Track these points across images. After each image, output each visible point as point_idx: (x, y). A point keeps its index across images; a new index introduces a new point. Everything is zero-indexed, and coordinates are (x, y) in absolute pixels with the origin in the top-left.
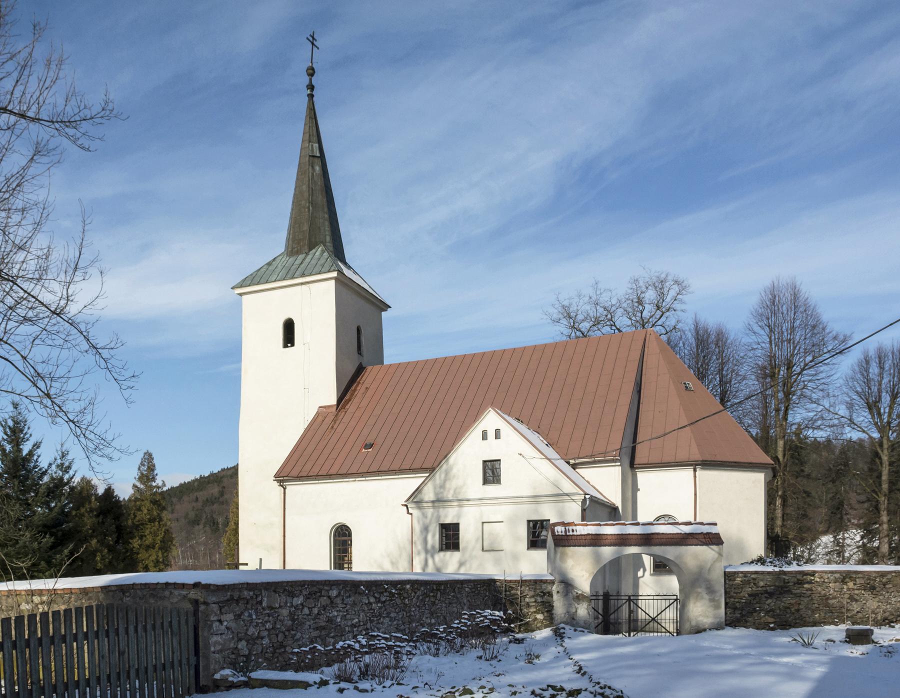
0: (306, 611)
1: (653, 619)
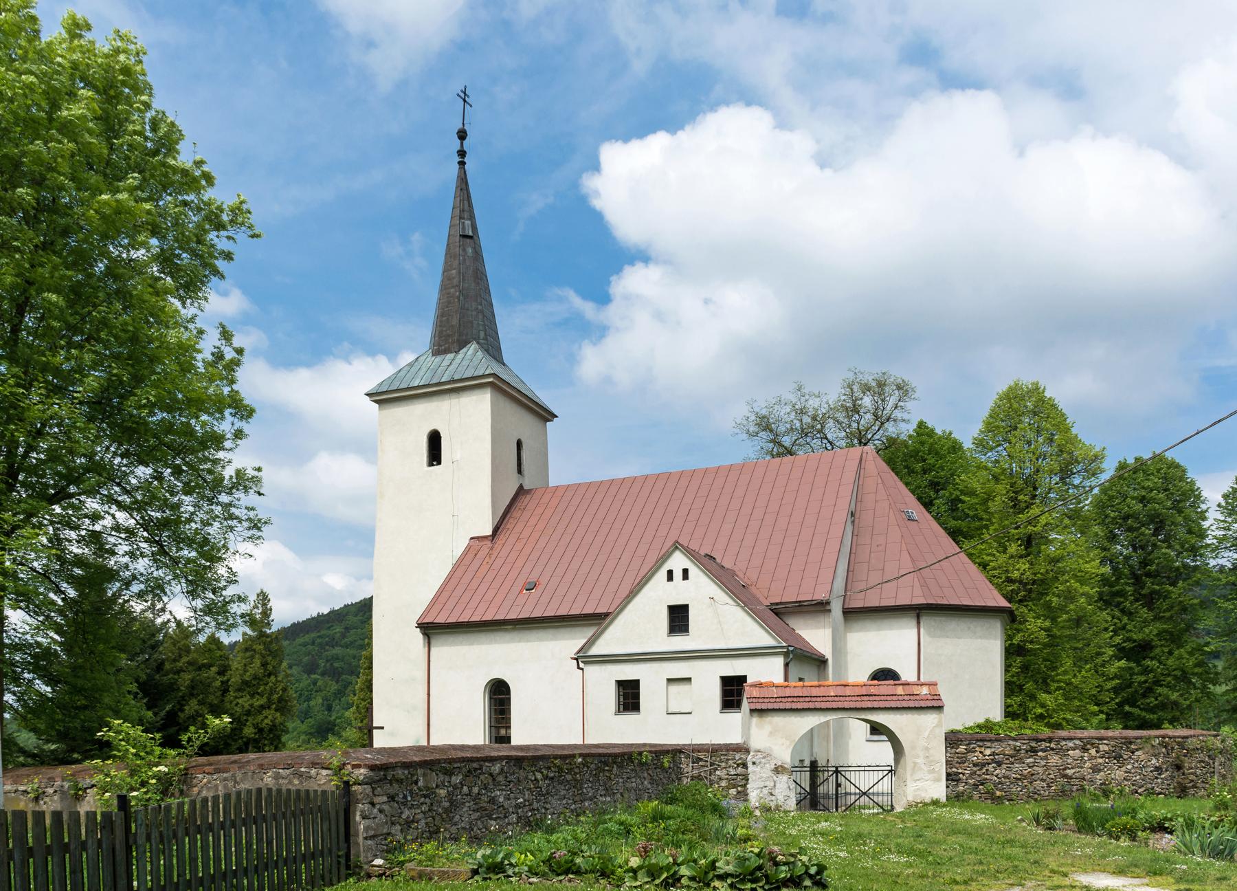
1: (864, 794)
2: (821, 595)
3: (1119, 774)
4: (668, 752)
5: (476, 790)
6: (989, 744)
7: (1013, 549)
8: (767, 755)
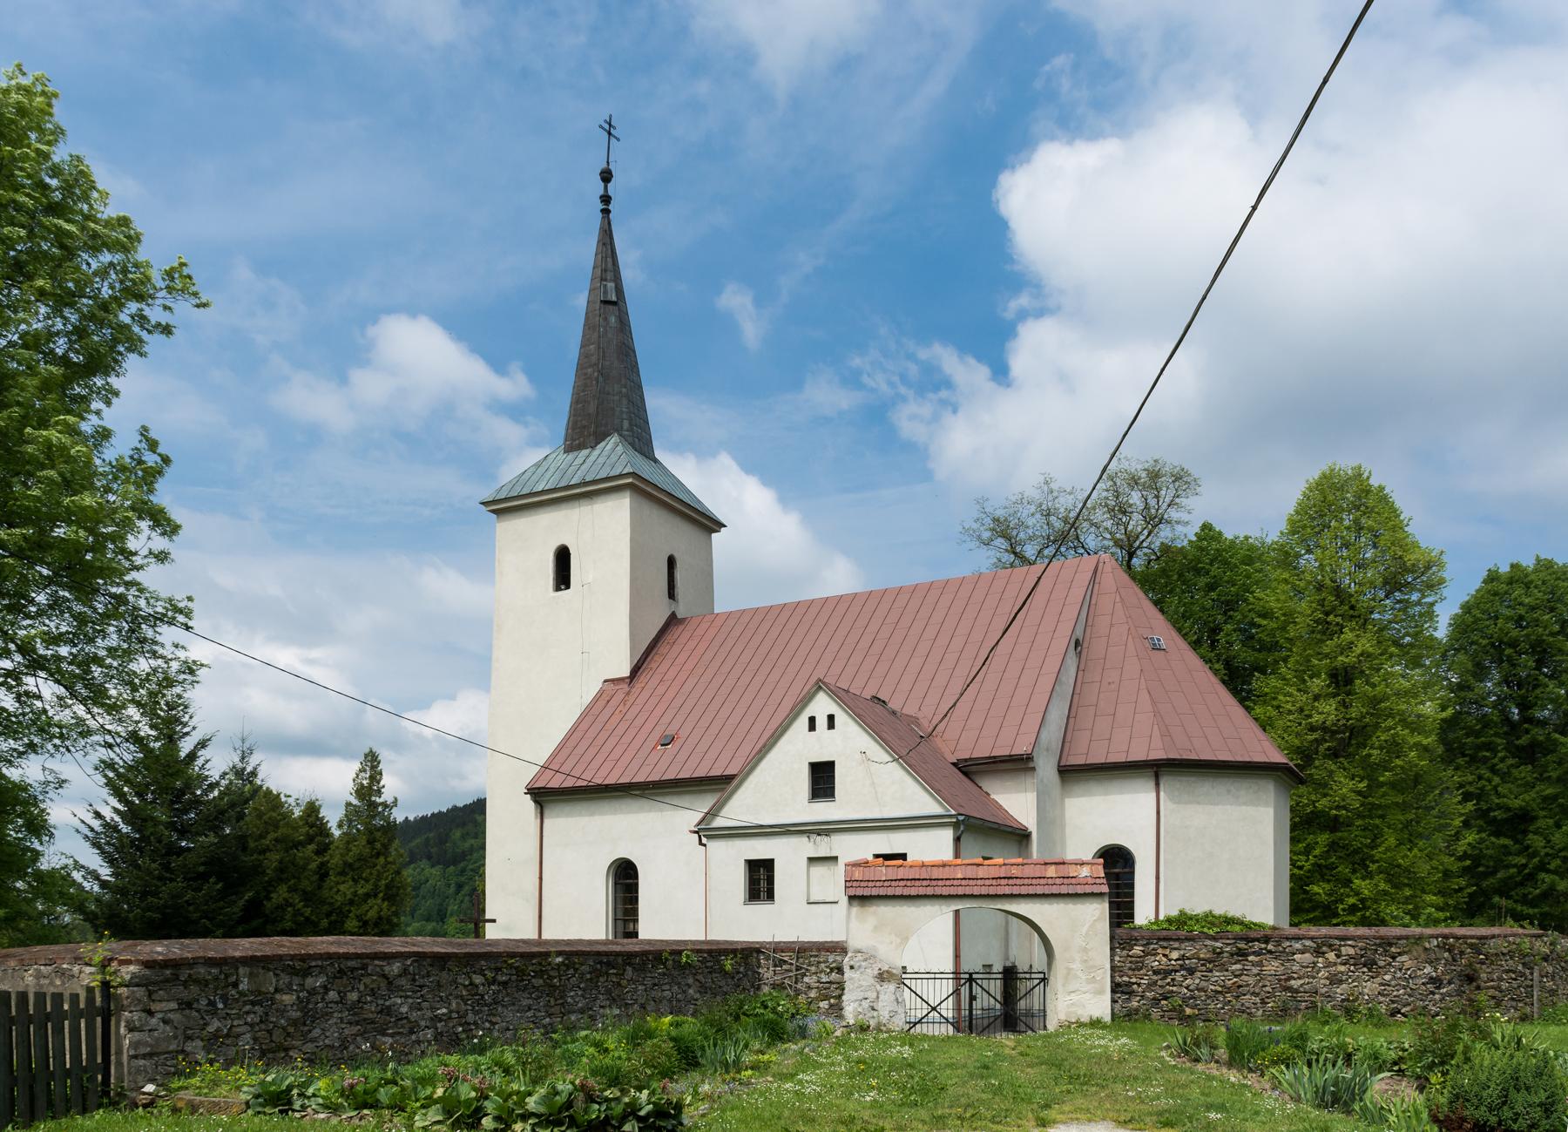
0: (332, 995)
2: (1021, 749)
3: (1370, 987)
4: (734, 951)
5: (354, 996)
6: (1176, 945)
7: (1318, 684)
8: (870, 957)
